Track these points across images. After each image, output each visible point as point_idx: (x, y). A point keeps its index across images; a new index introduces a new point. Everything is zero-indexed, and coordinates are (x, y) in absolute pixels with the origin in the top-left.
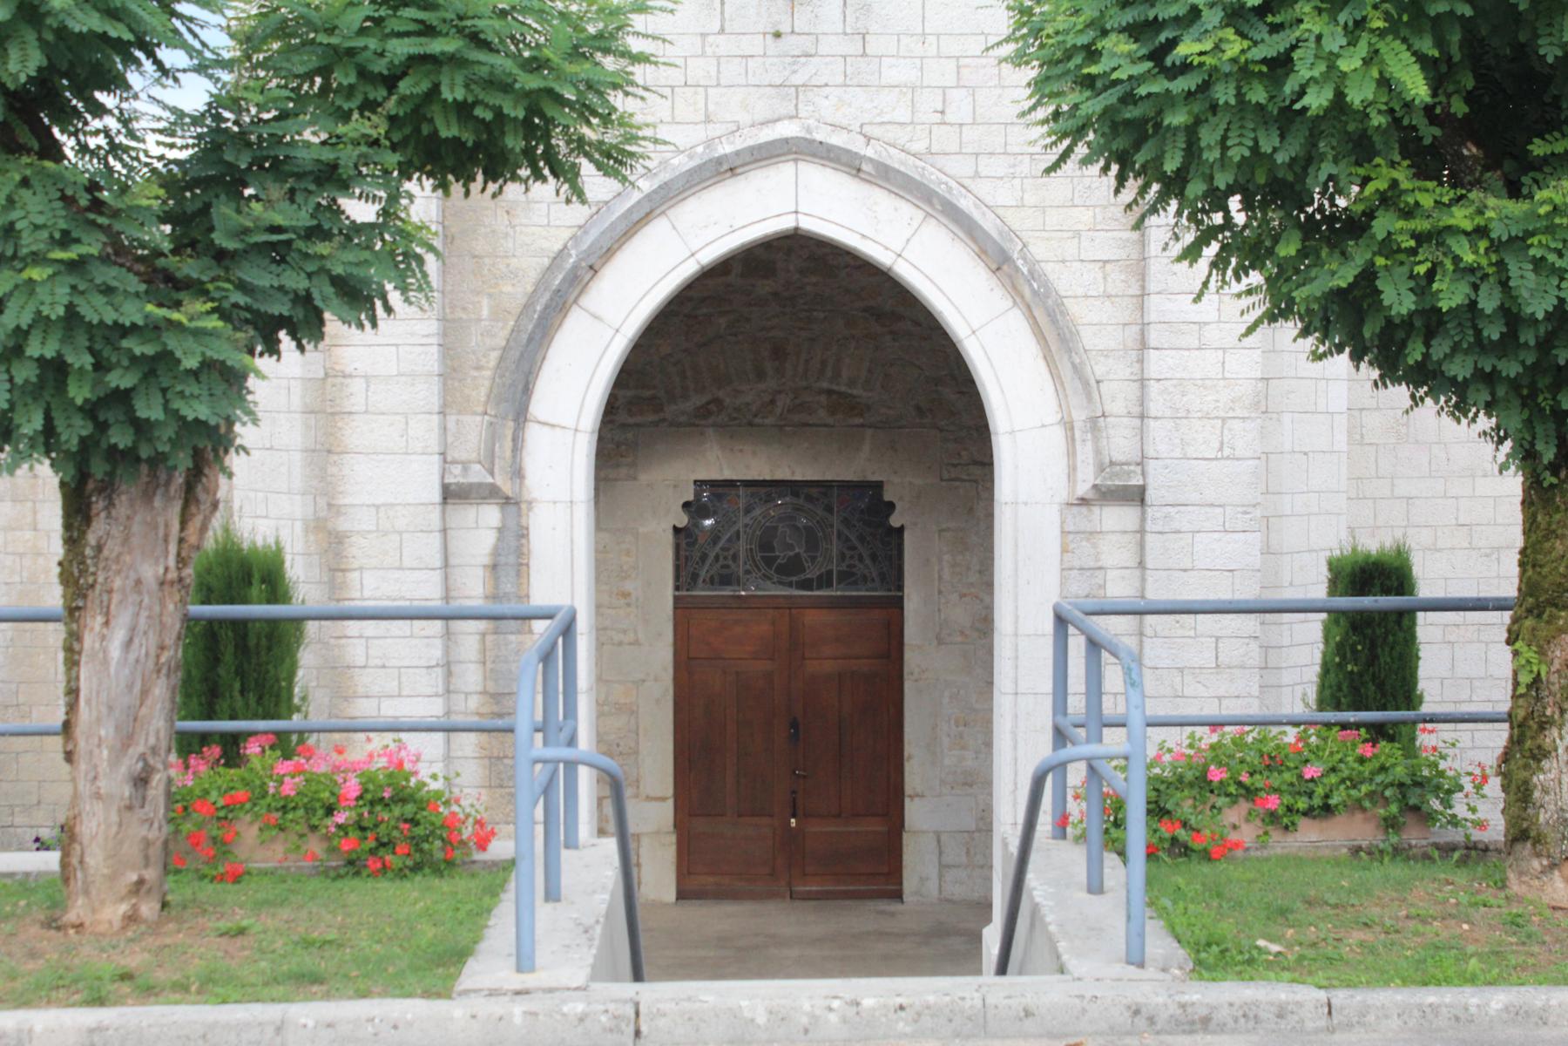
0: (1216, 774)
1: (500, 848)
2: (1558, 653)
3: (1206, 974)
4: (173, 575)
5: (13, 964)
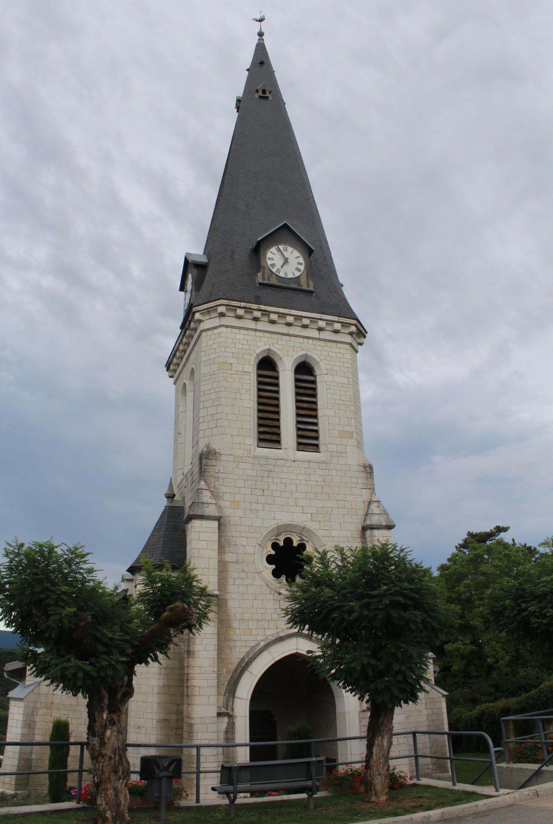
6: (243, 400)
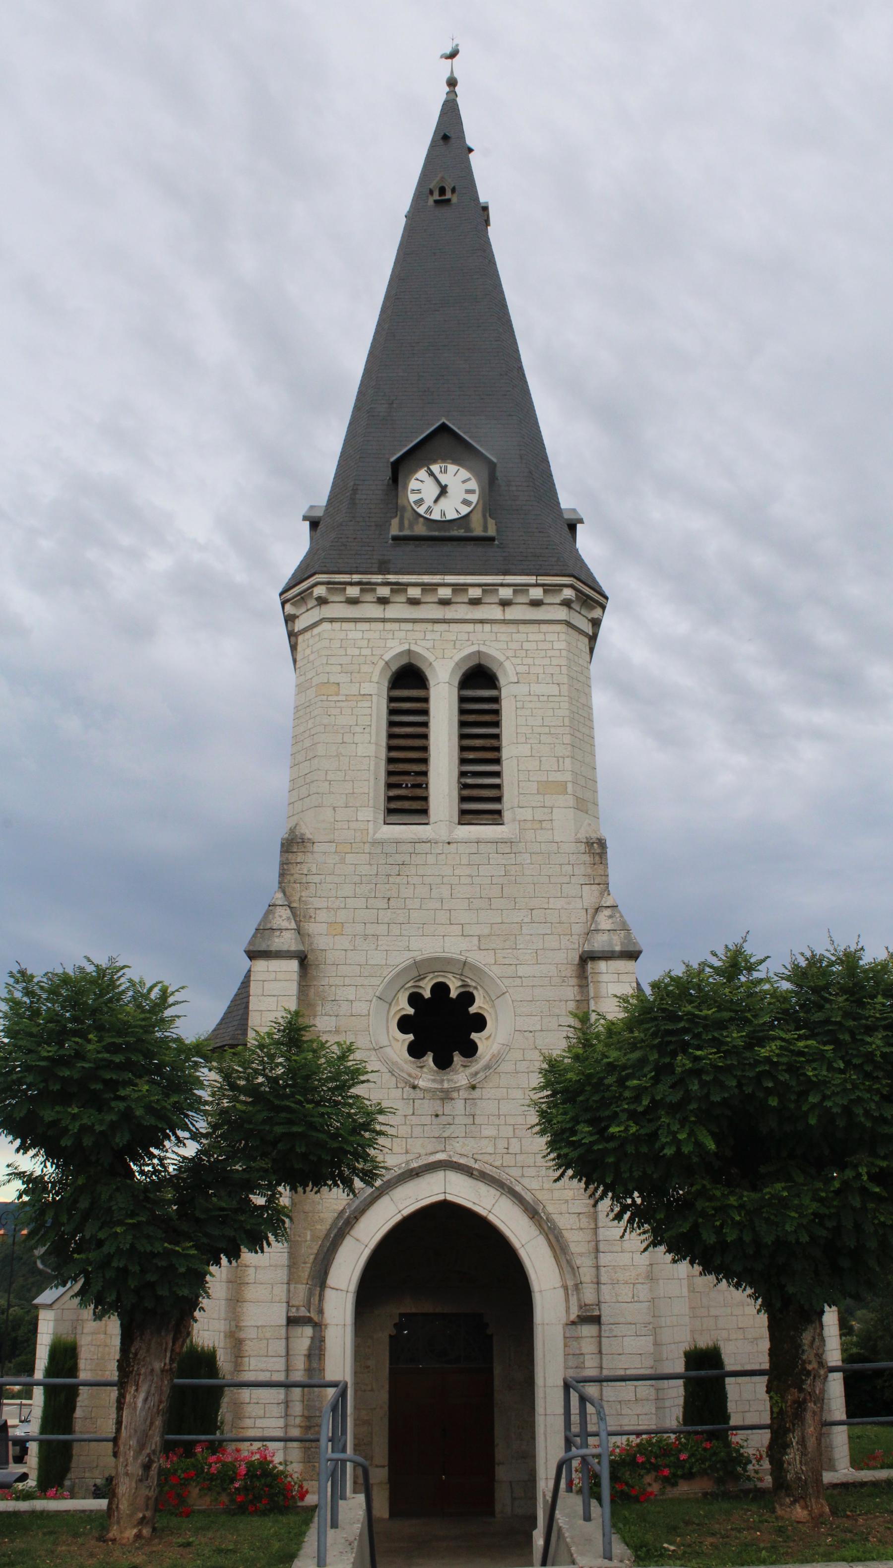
0: (640, 1459)
1: (311, 1499)
2: (789, 1397)
3: (641, 1563)
4: (167, 1367)
5: (82, 1560)
6: (356, 744)
